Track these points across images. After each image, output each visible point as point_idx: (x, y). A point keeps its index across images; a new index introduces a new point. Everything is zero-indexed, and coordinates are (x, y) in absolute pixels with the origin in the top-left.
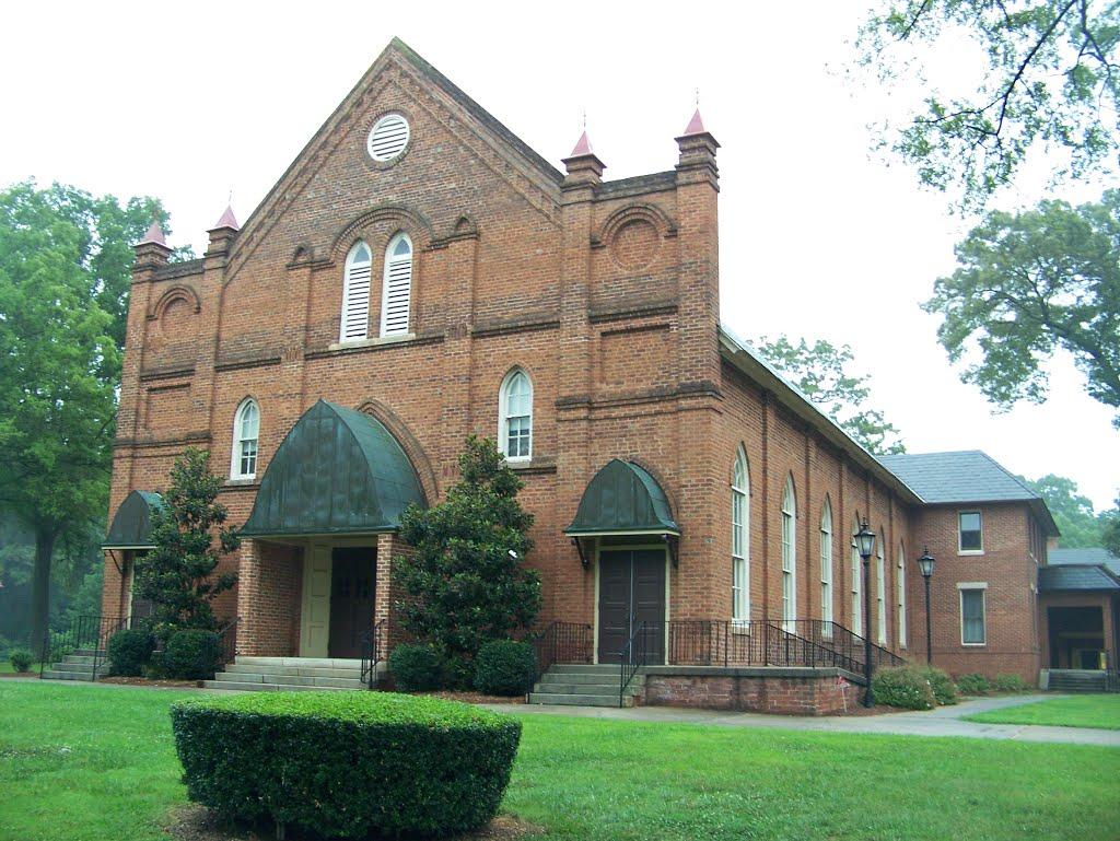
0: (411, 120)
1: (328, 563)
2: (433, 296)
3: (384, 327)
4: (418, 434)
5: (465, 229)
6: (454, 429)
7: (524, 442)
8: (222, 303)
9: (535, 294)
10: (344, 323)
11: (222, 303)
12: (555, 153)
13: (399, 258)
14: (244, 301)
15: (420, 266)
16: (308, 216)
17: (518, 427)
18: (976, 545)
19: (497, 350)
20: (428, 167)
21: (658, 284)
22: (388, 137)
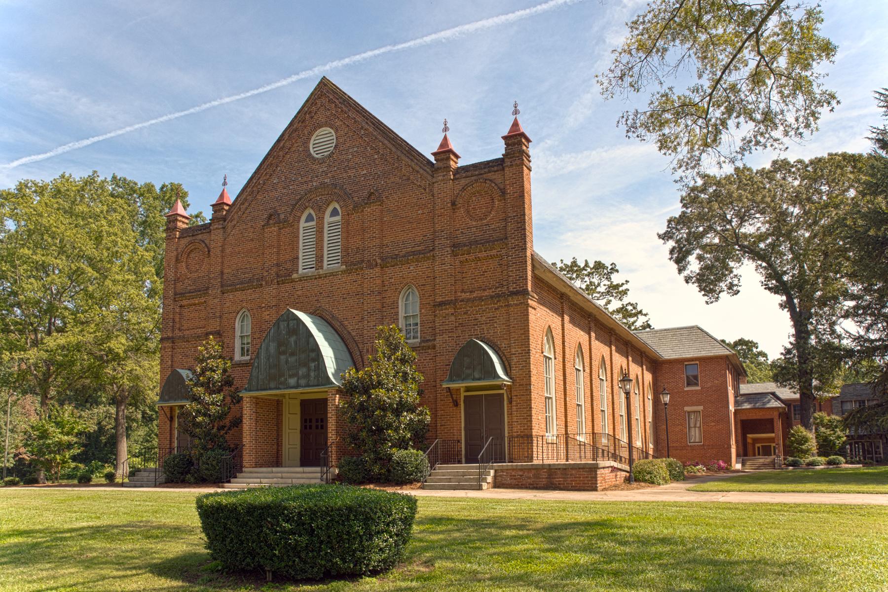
0: (336, 131)
1: (298, 410)
3: (325, 263)
4: (350, 328)
5: (372, 197)
8: (223, 251)
10: (301, 261)
12: (428, 149)
15: (346, 224)
20: (349, 161)
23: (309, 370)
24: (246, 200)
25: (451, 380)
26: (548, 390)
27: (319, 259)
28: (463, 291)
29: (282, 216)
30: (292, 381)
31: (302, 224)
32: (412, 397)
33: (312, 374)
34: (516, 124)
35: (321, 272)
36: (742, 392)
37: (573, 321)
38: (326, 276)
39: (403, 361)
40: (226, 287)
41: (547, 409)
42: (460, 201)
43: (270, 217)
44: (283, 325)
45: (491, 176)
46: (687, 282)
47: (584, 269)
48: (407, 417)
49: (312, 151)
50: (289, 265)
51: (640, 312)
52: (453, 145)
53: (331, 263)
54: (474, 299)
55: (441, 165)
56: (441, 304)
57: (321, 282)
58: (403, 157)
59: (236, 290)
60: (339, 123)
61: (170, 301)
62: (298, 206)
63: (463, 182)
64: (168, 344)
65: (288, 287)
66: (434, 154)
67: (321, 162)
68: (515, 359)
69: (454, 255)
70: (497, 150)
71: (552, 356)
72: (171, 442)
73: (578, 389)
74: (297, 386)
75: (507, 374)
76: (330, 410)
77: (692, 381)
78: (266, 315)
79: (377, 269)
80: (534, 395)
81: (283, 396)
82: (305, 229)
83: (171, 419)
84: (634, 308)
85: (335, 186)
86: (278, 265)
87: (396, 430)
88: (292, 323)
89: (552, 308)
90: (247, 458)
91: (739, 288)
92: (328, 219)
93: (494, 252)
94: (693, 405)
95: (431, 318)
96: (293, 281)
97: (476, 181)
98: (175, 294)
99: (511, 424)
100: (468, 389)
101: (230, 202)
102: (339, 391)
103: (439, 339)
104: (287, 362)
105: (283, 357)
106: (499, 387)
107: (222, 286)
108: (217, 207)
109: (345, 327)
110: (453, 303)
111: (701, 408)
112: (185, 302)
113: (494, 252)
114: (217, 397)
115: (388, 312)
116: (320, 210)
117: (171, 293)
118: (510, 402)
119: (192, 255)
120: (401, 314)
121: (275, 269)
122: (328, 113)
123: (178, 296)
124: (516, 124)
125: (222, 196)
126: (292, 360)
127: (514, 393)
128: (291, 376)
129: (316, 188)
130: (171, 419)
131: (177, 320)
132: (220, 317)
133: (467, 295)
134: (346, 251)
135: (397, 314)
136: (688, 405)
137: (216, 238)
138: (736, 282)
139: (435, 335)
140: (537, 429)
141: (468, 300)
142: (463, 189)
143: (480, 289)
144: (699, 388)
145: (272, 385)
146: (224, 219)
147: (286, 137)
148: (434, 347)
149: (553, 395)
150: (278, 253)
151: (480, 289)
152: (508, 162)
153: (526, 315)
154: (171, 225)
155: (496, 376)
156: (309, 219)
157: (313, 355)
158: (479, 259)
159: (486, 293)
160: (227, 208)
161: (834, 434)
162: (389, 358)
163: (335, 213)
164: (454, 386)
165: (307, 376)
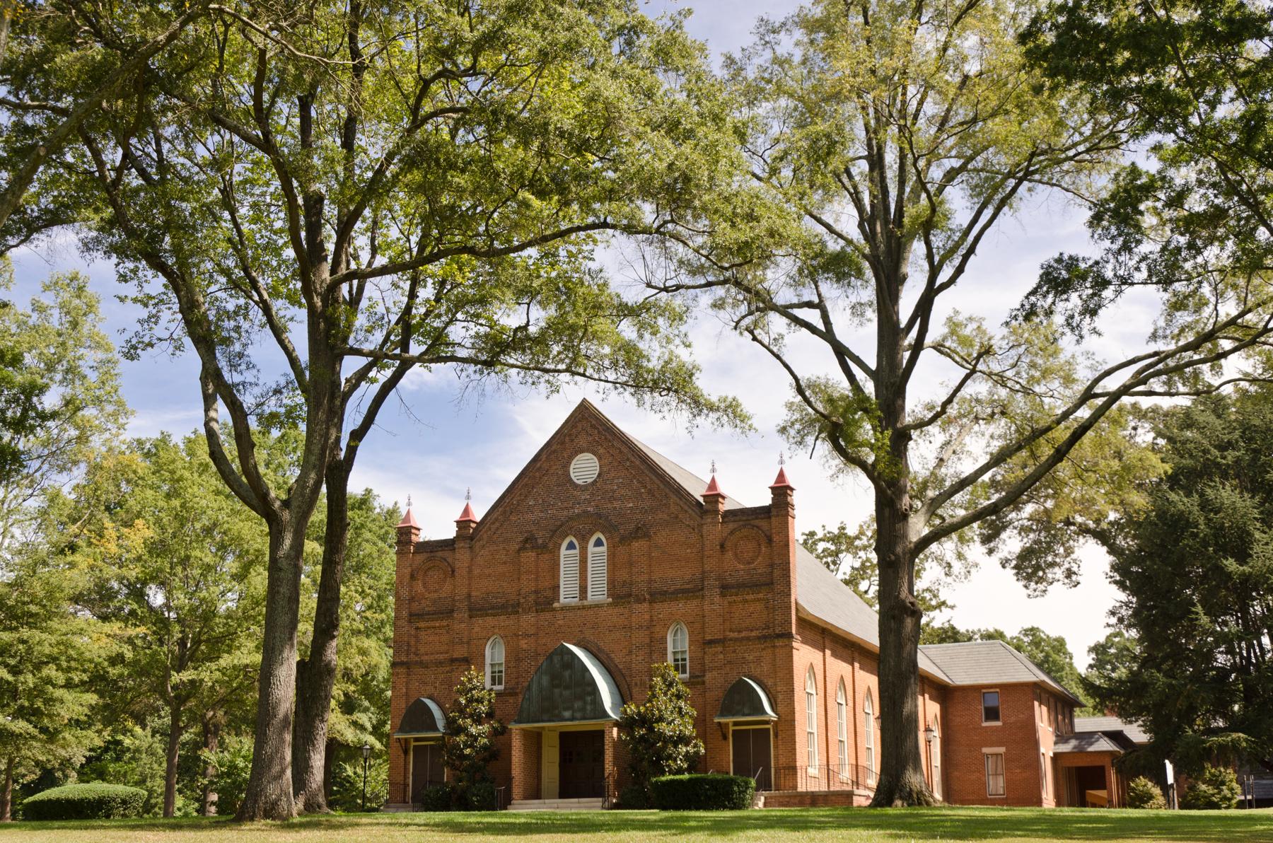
0: (600, 459)
1: (557, 742)
2: (623, 575)
3: (589, 594)
4: (617, 661)
5: (640, 532)
6: (640, 658)
7: (684, 666)
8: (470, 571)
9: (687, 577)
10: (562, 590)
11: (470, 571)
12: (698, 492)
13: (598, 554)
14: (487, 571)
15: (612, 556)
16: (530, 517)
17: (679, 657)
18: (996, 718)
19: (663, 609)
20: (614, 491)
21: (761, 575)
22: (584, 468)
23: (585, 703)
24: (496, 519)
25: (722, 715)
26: (810, 725)
27: (583, 590)
28: (731, 630)
29: (540, 541)
30: (567, 714)
31: (563, 551)
32: (689, 730)
33: (589, 707)
34: (781, 476)
35: (585, 603)
36: (1078, 729)
37: (834, 655)
38: (590, 607)
39: (679, 697)
40: (477, 610)
41: (809, 743)
42: (728, 544)
43: (526, 541)
44: (556, 659)
45: (757, 522)
46: (1004, 567)
47: (857, 538)
48: (683, 749)
49: (572, 475)
50: (549, 593)
51: (944, 603)
52: (722, 488)
53: (598, 592)
54: (742, 639)
55: (709, 507)
56: (711, 642)
57: (584, 612)
58: (671, 495)
59: (487, 615)
60: (602, 451)
61: (403, 623)
62: (558, 532)
63: (731, 526)
64: (402, 670)
65: (548, 615)
66: (704, 496)
67: (584, 488)
68: (780, 697)
69: (723, 595)
70: (764, 499)
71: (814, 692)
72: (406, 777)
73: (840, 725)
74: (572, 719)
75: (773, 710)
76: (606, 742)
77: (992, 714)
78: (523, 644)
79: (646, 605)
80: (798, 730)
81: (543, 728)
82: (566, 556)
83: (406, 752)
84: (935, 596)
85: (599, 516)
86: (536, 592)
87: (675, 760)
88: (566, 658)
89: (814, 645)
90: (517, 790)
91: (1079, 579)
92: (591, 548)
93: (761, 596)
94: (991, 746)
95: (700, 655)
96: (554, 610)
97: (744, 526)
98: (411, 615)
99: (776, 757)
100: (736, 724)
101: (478, 519)
102: (617, 724)
103: (708, 676)
104: (561, 695)
105: (557, 691)
106: (767, 722)
107: (470, 610)
108: (463, 524)
109: (612, 660)
110: (722, 641)
111: (1002, 750)
112: (422, 625)
113: (761, 596)
114: (485, 728)
115: (656, 647)
116: (584, 539)
117: (405, 613)
118: (776, 735)
119: (430, 573)
120: (670, 649)
121: (533, 597)
122: (590, 439)
123: (414, 617)
124: (781, 476)
125: (466, 511)
126: (567, 693)
127: (780, 728)
128: (566, 709)
129: (578, 515)
130: (406, 752)
131: (413, 643)
132: (468, 643)
133: (735, 635)
134: (612, 584)
135: (666, 649)
136: (986, 746)
137: (462, 558)
138: (1075, 569)
139: (704, 671)
140: (801, 761)
141: (736, 640)
142: (732, 533)
143: (747, 629)
144: (999, 724)
145: (545, 717)
146: (472, 538)
147: (544, 457)
148: (703, 683)
149: (815, 730)
150: (536, 580)
151: (747, 629)
152: (774, 512)
153: (791, 656)
154: (404, 538)
155: (764, 712)
156: (571, 546)
157: (589, 689)
158: (746, 601)
159: (753, 634)
160: (473, 525)
161: (1219, 793)
162: (665, 694)
163: (599, 543)
164: (723, 720)
165: (583, 709)
